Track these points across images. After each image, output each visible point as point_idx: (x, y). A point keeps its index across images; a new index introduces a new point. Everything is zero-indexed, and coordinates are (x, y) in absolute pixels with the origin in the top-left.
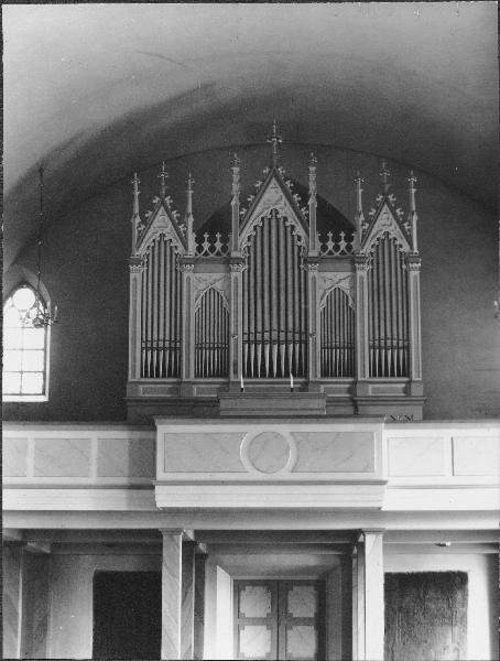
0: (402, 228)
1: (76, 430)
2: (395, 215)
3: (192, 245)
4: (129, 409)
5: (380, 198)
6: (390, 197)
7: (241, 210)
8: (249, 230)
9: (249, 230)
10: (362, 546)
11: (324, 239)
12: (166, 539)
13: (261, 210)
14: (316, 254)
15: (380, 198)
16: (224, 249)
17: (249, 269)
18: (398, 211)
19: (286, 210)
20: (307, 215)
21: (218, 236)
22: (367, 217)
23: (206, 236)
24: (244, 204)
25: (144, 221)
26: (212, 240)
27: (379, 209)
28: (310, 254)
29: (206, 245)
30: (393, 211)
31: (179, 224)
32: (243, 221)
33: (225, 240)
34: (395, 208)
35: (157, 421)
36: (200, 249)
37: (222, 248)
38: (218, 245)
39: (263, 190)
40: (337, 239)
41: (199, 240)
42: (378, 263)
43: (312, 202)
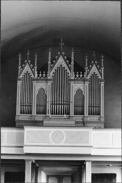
2: (30, 66)
3: (36, 75)
6: (96, 62)
8: (53, 71)
9: (53, 71)
10: (85, 165)
11: (76, 74)
13: (57, 65)
14: (73, 78)
17: (53, 82)
19: (64, 65)
20: (71, 67)
21: (78, 73)
24: (52, 63)
26: (42, 74)
28: (71, 78)
31: (33, 68)
32: (52, 68)
33: (46, 73)
35: (24, 127)
36: (38, 76)
41: (38, 73)
43: (72, 63)
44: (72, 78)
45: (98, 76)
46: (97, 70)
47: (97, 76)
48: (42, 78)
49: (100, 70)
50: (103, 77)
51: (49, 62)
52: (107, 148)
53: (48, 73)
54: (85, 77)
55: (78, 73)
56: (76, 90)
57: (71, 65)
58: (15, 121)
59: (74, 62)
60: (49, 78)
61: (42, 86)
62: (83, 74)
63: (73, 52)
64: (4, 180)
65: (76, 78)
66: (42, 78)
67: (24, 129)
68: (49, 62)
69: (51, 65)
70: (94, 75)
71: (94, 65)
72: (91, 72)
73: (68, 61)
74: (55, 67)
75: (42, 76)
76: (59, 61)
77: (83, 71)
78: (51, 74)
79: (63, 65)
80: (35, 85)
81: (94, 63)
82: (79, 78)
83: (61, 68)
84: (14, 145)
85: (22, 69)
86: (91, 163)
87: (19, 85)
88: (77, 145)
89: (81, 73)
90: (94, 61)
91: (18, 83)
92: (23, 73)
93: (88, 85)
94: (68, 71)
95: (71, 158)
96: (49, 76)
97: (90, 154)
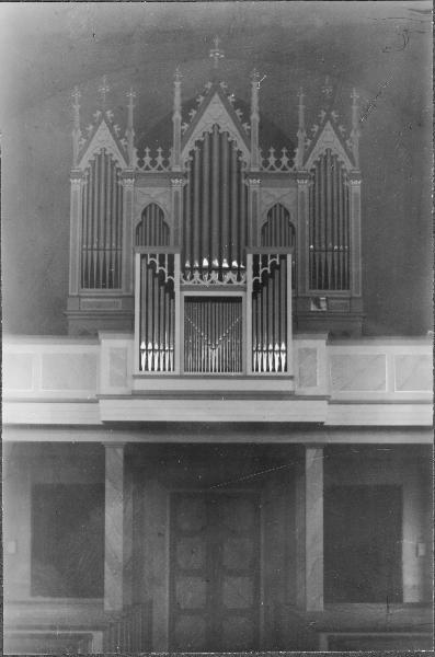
0: (345, 146)
1: (115, 338)
2: (112, 130)
3: (135, 160)
4: (70, 323)
5: (324, 114)
6: (108, 112)
7: (182, 124)
8: (190, 146)
9: (190, 146)
10: (303, 459)
11: (265, 155)
12: (108, 450)
13: (204, 125)
14: (257, 170)
15: (99, 113)
16: (166, 163)
17: (88, 185)
18: (115, 126)
19: (228, 125)
20: (249, 131)
21: (284, 151)
22: (309, 132)
23: (147, 150)
24: (186, 118)
25: (310, 135)
26: (154, 155)
27: (96, 126)
28: (252, 170)
29: (147, 159)
30: (111, 127)
31: (121, 138)
32: (184, 138)
33: (166, 154)
34: (113, 124)
35: (101, 335)
36: (141, 163)
37: (163, 162)
38: (160, 160)
39: (206, 103)
40: (278, 155)
41: (141, 154)
42: (93, 178)
43: (255, 117)
44: (255, 169)
45: (342, 163)
46: (337, 140)
47: (107, 153)
48: (154, 170)
49: (347, 142)
50: (357, 163)
51: (177, 116)
52: (389, 403)
53: (173, 151)
54: (296, 165)
55: (275, 153)
56: (269, 208)
57: (249, 124)
58: (65, 315)
59: (260, 113)
60: (177, 169)
61: (278, 196)
62: (291, 155)
63: (180, 79)
64: (29, 521)
65: (266, 170)
66: (154, 170)
67: (99, 343)
68: (177, 116)
69: (182, 124)
70: (328, 159)
71: (103, 122)
72: (316, 149)
73: (238, 113)
74: (197, 135)
75: (153, 163)
76: (209, 110)
77: (291, 147)
78: (185, 156)
79: (222, 126)
80: (255, 194)
81: (328, 117)
82: (278, 167)
83: (216, 138)
84: (42, 393)
85: (84, 141)
86: (321, 451)
87: (75, 192)
88: (204, 381)
89: (272, 150)
90: (328, 112)
91: (73, 188)
92: (89, 156)
93: (306, 192)
94: (241, 145)
95: (281, 437)
96: (177, 164)
97: (322, 423)
